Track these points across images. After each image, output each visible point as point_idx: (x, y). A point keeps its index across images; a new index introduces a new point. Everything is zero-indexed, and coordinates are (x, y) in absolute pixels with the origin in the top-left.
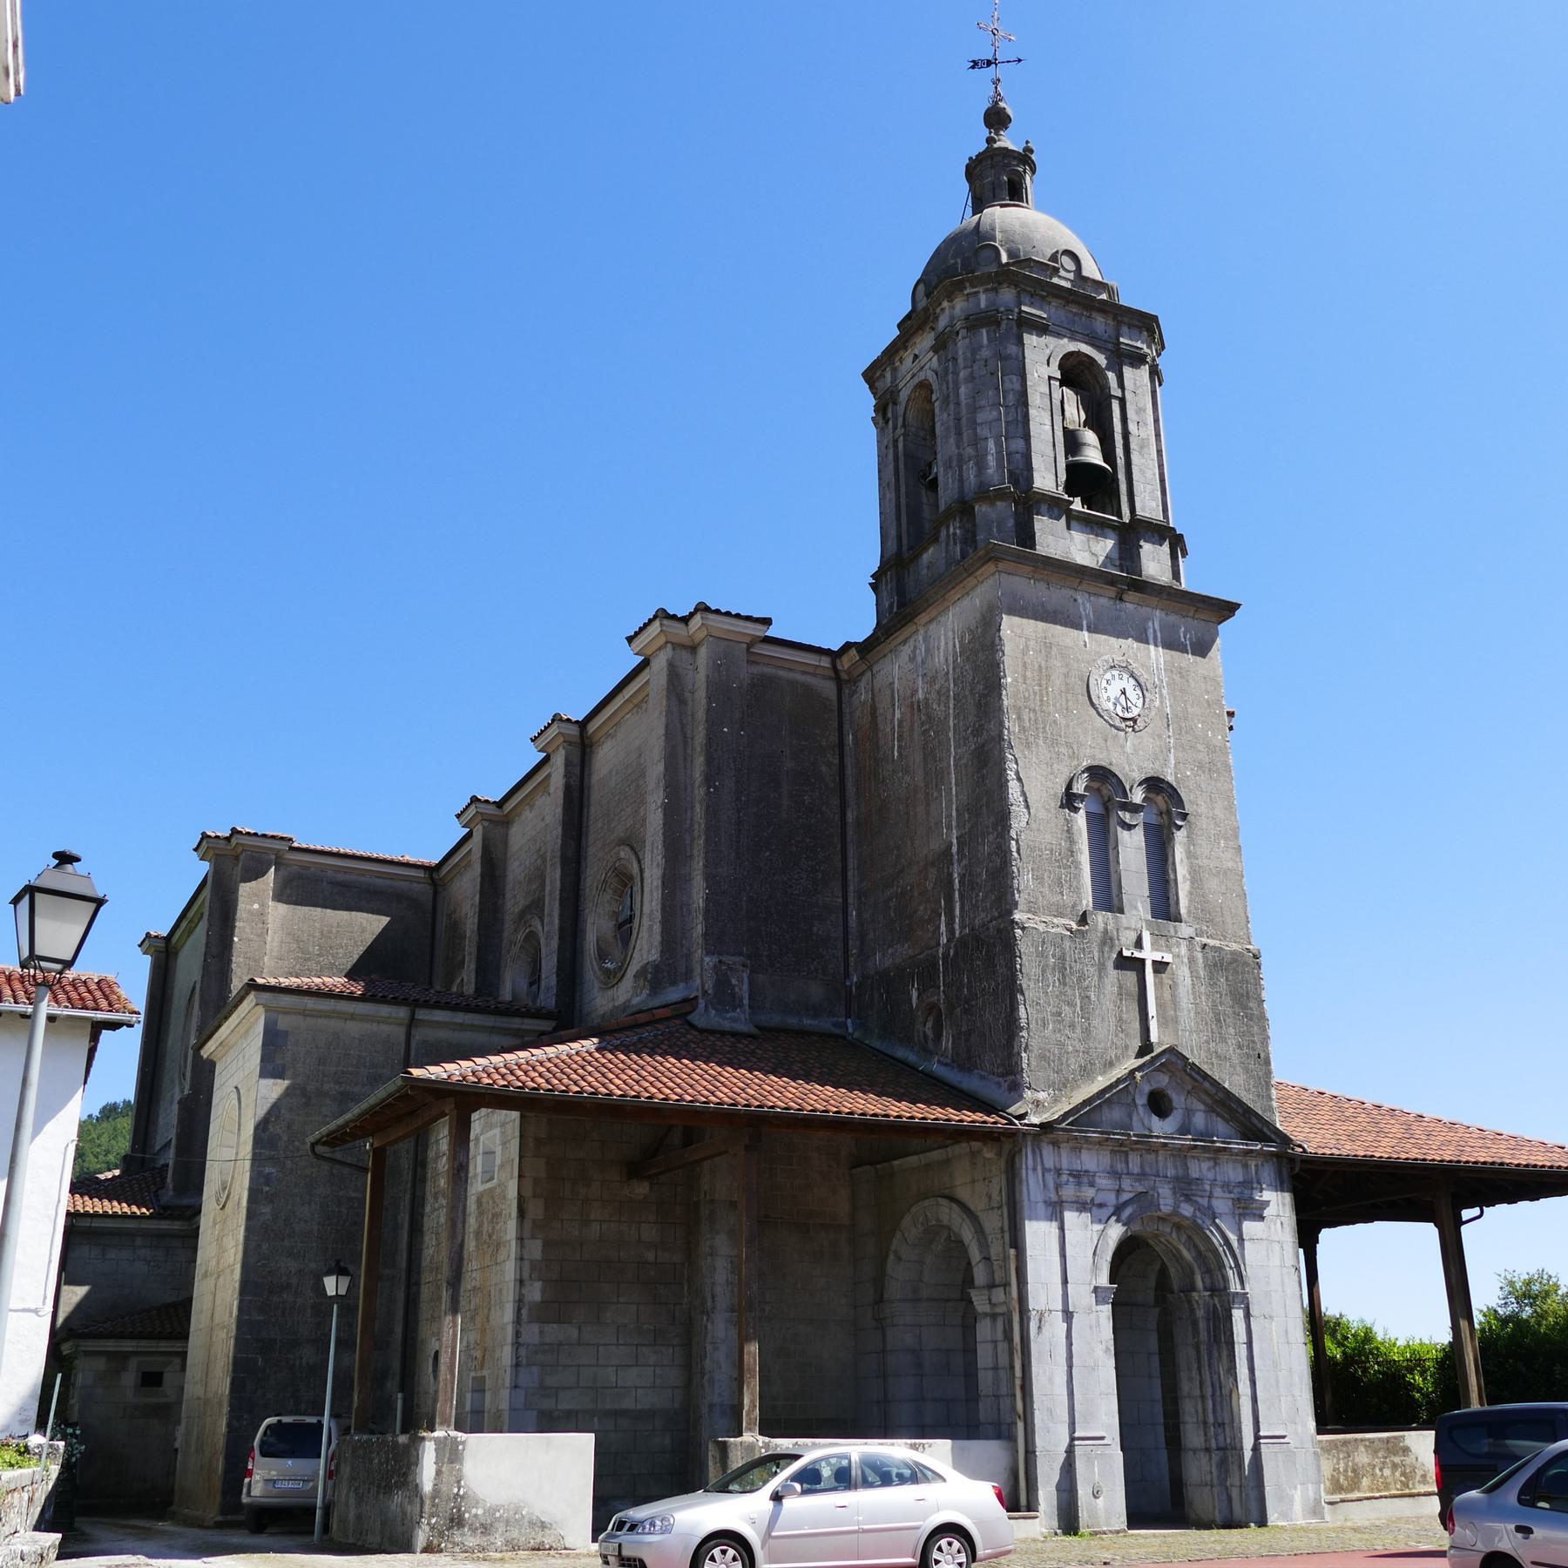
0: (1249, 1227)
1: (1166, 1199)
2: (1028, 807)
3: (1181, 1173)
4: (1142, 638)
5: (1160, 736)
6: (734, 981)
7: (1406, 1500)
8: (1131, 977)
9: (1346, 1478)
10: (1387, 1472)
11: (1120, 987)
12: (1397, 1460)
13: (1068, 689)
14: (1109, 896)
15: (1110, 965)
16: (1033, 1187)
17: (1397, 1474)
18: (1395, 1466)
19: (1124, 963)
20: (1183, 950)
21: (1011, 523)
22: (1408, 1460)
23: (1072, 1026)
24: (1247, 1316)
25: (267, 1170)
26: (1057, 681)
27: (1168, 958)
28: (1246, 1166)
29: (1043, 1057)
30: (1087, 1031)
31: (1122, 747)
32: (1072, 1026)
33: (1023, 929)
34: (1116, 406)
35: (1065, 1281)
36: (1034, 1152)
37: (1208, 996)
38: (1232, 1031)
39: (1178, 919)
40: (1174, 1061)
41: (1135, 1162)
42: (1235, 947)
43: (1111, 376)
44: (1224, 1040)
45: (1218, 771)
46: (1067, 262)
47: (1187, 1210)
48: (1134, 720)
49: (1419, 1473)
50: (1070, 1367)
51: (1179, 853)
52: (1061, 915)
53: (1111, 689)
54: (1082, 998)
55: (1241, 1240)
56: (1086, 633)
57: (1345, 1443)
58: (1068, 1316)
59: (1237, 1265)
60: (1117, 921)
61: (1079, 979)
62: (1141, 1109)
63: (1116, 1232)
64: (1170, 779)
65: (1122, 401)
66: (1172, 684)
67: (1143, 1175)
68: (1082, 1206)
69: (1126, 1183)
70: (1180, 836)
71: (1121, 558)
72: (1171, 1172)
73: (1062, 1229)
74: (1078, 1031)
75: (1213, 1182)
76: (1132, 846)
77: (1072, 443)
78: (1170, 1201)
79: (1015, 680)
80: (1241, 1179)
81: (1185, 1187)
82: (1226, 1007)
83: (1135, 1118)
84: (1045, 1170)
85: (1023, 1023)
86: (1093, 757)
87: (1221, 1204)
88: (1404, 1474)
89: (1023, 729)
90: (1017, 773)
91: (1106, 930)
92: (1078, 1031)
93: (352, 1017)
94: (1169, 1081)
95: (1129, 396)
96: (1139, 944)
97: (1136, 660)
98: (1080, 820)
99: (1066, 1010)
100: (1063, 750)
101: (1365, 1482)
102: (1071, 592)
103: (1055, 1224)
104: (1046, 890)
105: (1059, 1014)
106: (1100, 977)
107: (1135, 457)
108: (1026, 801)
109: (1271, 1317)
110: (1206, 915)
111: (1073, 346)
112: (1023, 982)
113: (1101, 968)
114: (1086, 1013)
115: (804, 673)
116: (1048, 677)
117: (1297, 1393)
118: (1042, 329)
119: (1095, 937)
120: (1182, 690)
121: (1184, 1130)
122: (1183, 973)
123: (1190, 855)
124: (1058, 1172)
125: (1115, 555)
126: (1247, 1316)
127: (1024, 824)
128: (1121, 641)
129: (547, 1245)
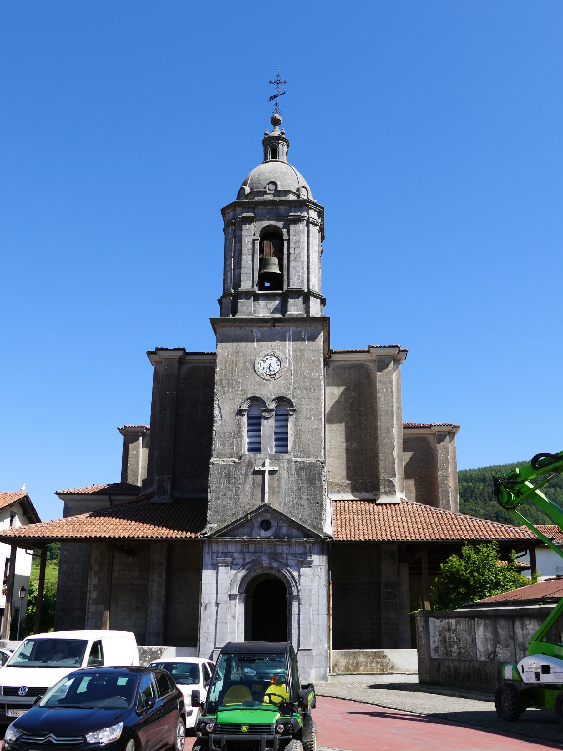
0: (303, 570)
1: (265, 561)
2: (221, 417)
3: (273, 551)
4: (283, 339)
5: (287, 379)
6: (165, 485)
7: (370, 675)
8: (260, 477)
9: (353, 666)
10: (373, 665)
11: (254, 482)
12: (379, 660)
13: (245, 367)
14: (256, 446)
15: (250, 474)
16: (207, 559)
17: (379, 666)
18: (378, 662)
19: (256, 473)
20: (286, 464)
21: (230, 305)
22: (385, 661)
23: (230, 499)
24: (299, 604)
25: (65, 553)
26: (240, 365)
27: (276, 468)
28: (305, 547)
29: (216, 511)
30: (237, 500)
31: (268, 387)
32: (230, 499)
33: (213, 464)
34: (285, 244)
35: (217, 593)
36: (208, 546)
37: (295, 482)
38: (305, 494)
39: (286, 451)
40: (267, 508)
41: (252, 548)
42: (312, 460)
43: (285, 231)
44: (301, 498)
45: (314, 389)
46: (272, 187)
47: (275, 565)
48: (275, 375)
49: (390, 666)
50: (216, 623)
51: (290, 425)
52: (232, 457)
53: (262, 366)
54: (236, 488)
55: (299, 575)
56: (256, 343)
57: (354, 653)
58: (217, 605)
59: (296, 585)
60: (255, 456)
61: (235, 481)
62: (256, 528)
63: (242, 573)
64: (290, 396)
65: (288, 241)
66: (295, 357)
67: (255, 552)
68: (226, 565)
69: (247, 556)
70: (291, 419)
71: (281, 307)
72: (268, 551)
73: (217, 573)
74: (233, 500)
75: (287, 554)
76: (268, 426)
77: (263, 263)
78: (268, 561)
79: (221, 369)
80: (302, 552)
81: (274, 556)
82: (304, 485)
83: (254, 531)
84: (213, 553)
85: (209, 499)
86: (254, 393)
87: (291, 562)
88: (382, 666)
89: (222, 387)
90: (218, 405)
91: (249, 461)
92: (233, 500)
93: (92, 500)
94: (266, 517)
95: (292, 238)
96: (264, 465)
97: (279, 350)
98: (245, 419)
99: (228, 493)
100: (240, 393)
101: (361, 668)
102: (251, 328)
103: (215, 572)
104: (226, 448)
105: (225, 495)
106: (245, 479)
107: (292, 264)
108: (221, 415)
109: (311, 605)
110: (301, 449)
111: (266, 223)
112: (210, 484)
113: (246, 475)
114: (237, 493)
115: (210, 363)
116: (236, 365)
117: (320, 633)
118: (250, 221)
119: (244, 465)
120: (300, 358)
121: (276, 535)
122: (284, 474)
123: (295, 425)
124: (218, 552)
125: (279, 307)
126: (299, 604)
127: (219, 424)
128: (273, 343)
129: (99, 579)
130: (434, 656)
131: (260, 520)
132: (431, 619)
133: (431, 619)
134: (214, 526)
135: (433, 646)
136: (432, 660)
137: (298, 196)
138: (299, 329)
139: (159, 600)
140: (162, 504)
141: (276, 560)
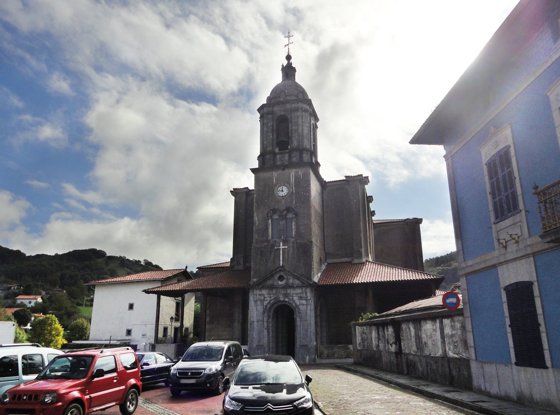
66: (295, 186)
129: (375, 351)
130: (359, 348)
131: (278, 275)
132: (357, 327)
133: (357, 327)
134: (255, 280)
135: (358, 342)
136: (358, 350)
137: (298, 97)
138: (297, 170)
139: (239, 321)
140: (239, 270)
141: (287, 297)
